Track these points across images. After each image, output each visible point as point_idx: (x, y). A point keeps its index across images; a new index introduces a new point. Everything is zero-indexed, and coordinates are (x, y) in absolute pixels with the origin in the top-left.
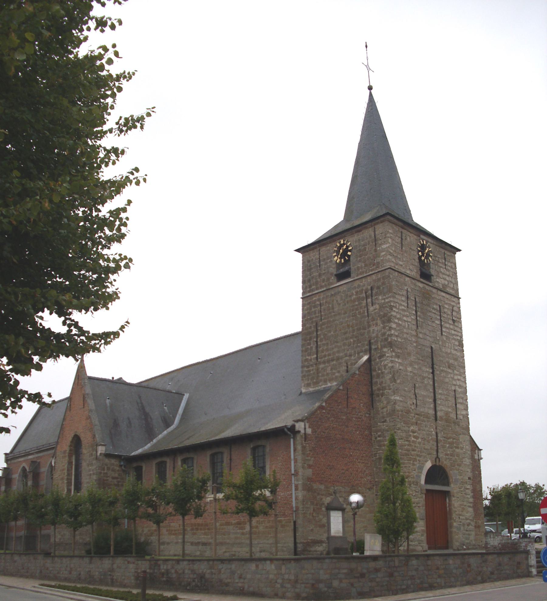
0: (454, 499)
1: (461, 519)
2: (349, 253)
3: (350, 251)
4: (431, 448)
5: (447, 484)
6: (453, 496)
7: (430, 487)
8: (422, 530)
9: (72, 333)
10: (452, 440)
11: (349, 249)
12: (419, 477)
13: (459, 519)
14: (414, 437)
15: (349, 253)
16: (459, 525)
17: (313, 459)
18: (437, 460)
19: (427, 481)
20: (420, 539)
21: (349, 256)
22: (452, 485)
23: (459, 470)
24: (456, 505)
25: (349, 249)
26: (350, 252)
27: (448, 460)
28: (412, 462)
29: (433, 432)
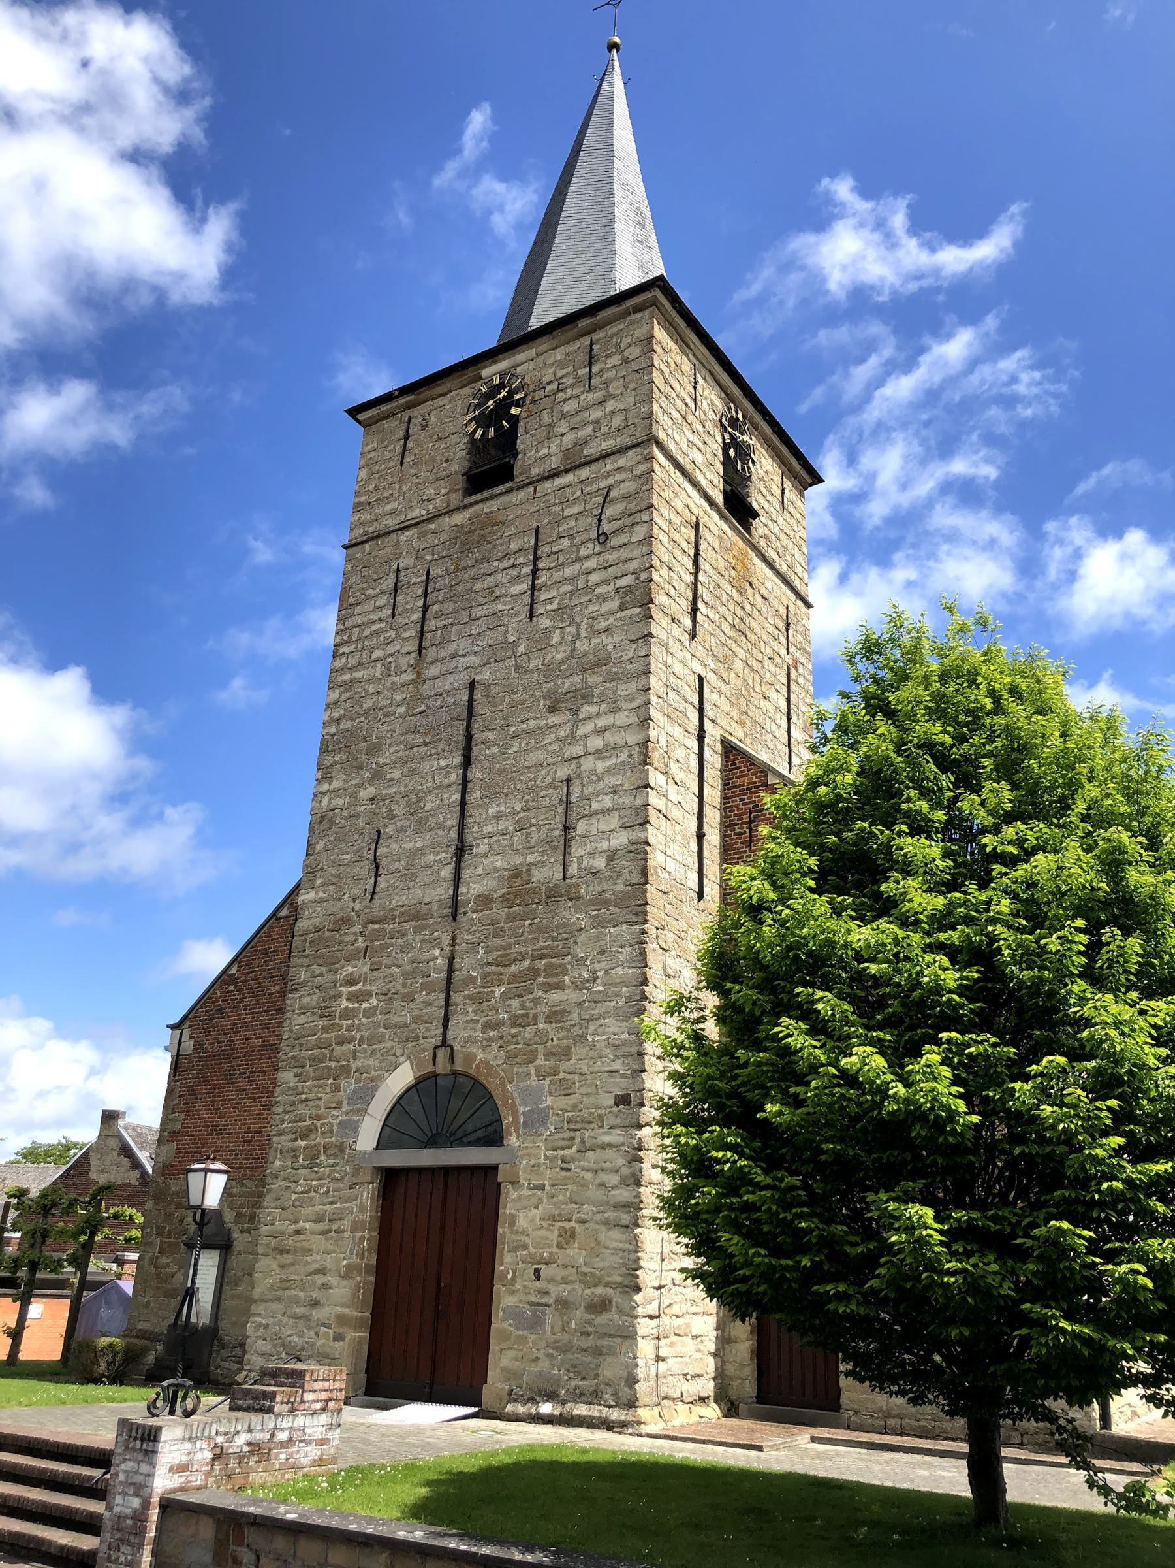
0: (514, 1194)
1: (551, 1280)
2: (515, 411)
3: (518, 404)
4: (417, 1019)
5: (494, 1137)
6: (515, 1183)
7: (396, 1158)
8: (342, 1320)
9: (1110, 671)
10: (527, 963)
11: (517, 397)
12: (352, 1127)
13: (538, 1278)
14: (352, 997)
15: (515, 411)
16: (531, 1304)
17: (183, 1116)
18: (442, 1054)
19: (387, 1140)
20: (328, 1350)
21: (514, 420)
22: (512, 1140)
23: (557, 1073)
24: (522, 1222)
25: (517, 397)
26: (518, 406)
27: (495, 1046)
28: (330, 1081)
29: (440, 961)
